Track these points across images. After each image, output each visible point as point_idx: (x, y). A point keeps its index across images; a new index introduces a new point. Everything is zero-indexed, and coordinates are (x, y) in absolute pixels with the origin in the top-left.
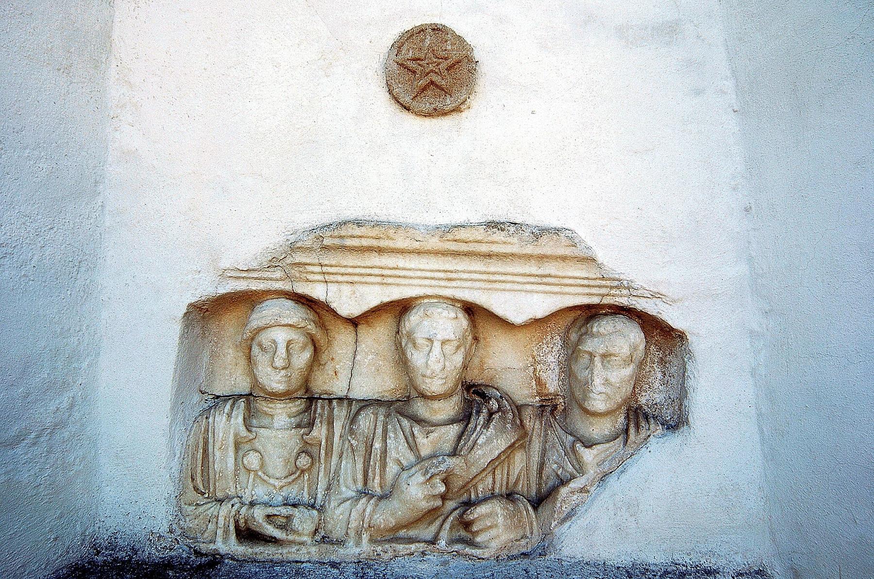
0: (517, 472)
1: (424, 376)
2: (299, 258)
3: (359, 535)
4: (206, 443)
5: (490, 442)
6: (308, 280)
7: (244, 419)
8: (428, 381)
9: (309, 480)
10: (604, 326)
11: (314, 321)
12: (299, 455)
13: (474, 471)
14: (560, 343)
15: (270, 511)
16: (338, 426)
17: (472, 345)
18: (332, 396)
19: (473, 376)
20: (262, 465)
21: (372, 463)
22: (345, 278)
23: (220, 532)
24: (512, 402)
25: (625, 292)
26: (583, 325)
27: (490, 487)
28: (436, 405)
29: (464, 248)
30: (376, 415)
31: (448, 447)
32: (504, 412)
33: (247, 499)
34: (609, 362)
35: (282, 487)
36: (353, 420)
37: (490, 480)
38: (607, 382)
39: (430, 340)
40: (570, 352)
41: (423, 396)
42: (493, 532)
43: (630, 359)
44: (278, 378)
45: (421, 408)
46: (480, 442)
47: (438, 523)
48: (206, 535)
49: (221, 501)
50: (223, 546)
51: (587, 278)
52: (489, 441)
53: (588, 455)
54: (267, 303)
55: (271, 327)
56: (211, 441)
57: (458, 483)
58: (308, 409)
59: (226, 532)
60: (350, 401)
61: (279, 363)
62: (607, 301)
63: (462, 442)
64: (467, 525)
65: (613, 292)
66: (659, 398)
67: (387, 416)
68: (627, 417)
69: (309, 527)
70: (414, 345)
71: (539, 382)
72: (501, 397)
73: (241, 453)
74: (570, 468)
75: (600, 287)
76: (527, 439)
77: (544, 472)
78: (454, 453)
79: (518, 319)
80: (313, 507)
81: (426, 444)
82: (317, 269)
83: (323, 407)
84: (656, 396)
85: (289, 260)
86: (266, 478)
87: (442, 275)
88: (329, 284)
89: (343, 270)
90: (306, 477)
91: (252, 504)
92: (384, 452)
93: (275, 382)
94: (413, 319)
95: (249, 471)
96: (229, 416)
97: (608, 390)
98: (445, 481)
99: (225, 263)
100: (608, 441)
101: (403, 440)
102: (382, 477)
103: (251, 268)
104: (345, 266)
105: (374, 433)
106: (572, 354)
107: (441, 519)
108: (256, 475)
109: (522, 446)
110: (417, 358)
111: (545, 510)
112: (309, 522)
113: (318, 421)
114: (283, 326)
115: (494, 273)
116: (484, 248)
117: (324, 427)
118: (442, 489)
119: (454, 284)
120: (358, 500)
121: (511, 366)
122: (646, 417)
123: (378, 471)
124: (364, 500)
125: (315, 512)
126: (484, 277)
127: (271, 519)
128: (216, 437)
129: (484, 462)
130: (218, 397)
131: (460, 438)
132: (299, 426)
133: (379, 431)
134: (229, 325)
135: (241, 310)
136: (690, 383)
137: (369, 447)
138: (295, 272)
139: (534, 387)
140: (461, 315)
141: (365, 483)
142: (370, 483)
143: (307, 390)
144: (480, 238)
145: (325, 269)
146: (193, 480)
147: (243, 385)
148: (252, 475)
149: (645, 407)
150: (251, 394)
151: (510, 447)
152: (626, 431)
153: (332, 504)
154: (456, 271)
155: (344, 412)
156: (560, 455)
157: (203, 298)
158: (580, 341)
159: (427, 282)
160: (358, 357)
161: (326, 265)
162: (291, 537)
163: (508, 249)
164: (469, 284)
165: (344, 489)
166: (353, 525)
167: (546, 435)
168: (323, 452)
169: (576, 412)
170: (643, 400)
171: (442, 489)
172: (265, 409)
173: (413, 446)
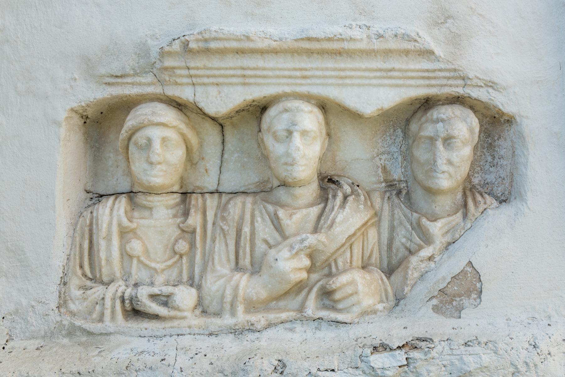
2: (169, 62)
3: (233, 306)
4: (91, 231)
6: (176, 84)
14: (402, 135)
18: (205, 191)
22: (211, 80)
37: (348, 254)
46: (338, 220)
49: (108, 284)
50: (111, 325)
51: (428, 71)
58: (184, 201)
67: (254, 203)
78: (316, 230)
82: (185, 72)
87: (298, 73)
89: (208, 72)
97: (451, 169)
98: (311, 256)
101: (269, 222)
107: (306, 290)
108: (140, 261)
111: (397, 277)
113: (192, 211)
129: (342, 239)
130: (101, 196)
133: (248, 217)
139: (381, 174)
140: (316, 110)
142: (241, 262)
147: (125, 186)
148: (135, 261)
152: (465, 205)
155: (215, 203)
156: (407, 230)
160: (226, 156)
161: (193, 68)
162: (173, 313)
165: (218, 267)
172: (145, 202)
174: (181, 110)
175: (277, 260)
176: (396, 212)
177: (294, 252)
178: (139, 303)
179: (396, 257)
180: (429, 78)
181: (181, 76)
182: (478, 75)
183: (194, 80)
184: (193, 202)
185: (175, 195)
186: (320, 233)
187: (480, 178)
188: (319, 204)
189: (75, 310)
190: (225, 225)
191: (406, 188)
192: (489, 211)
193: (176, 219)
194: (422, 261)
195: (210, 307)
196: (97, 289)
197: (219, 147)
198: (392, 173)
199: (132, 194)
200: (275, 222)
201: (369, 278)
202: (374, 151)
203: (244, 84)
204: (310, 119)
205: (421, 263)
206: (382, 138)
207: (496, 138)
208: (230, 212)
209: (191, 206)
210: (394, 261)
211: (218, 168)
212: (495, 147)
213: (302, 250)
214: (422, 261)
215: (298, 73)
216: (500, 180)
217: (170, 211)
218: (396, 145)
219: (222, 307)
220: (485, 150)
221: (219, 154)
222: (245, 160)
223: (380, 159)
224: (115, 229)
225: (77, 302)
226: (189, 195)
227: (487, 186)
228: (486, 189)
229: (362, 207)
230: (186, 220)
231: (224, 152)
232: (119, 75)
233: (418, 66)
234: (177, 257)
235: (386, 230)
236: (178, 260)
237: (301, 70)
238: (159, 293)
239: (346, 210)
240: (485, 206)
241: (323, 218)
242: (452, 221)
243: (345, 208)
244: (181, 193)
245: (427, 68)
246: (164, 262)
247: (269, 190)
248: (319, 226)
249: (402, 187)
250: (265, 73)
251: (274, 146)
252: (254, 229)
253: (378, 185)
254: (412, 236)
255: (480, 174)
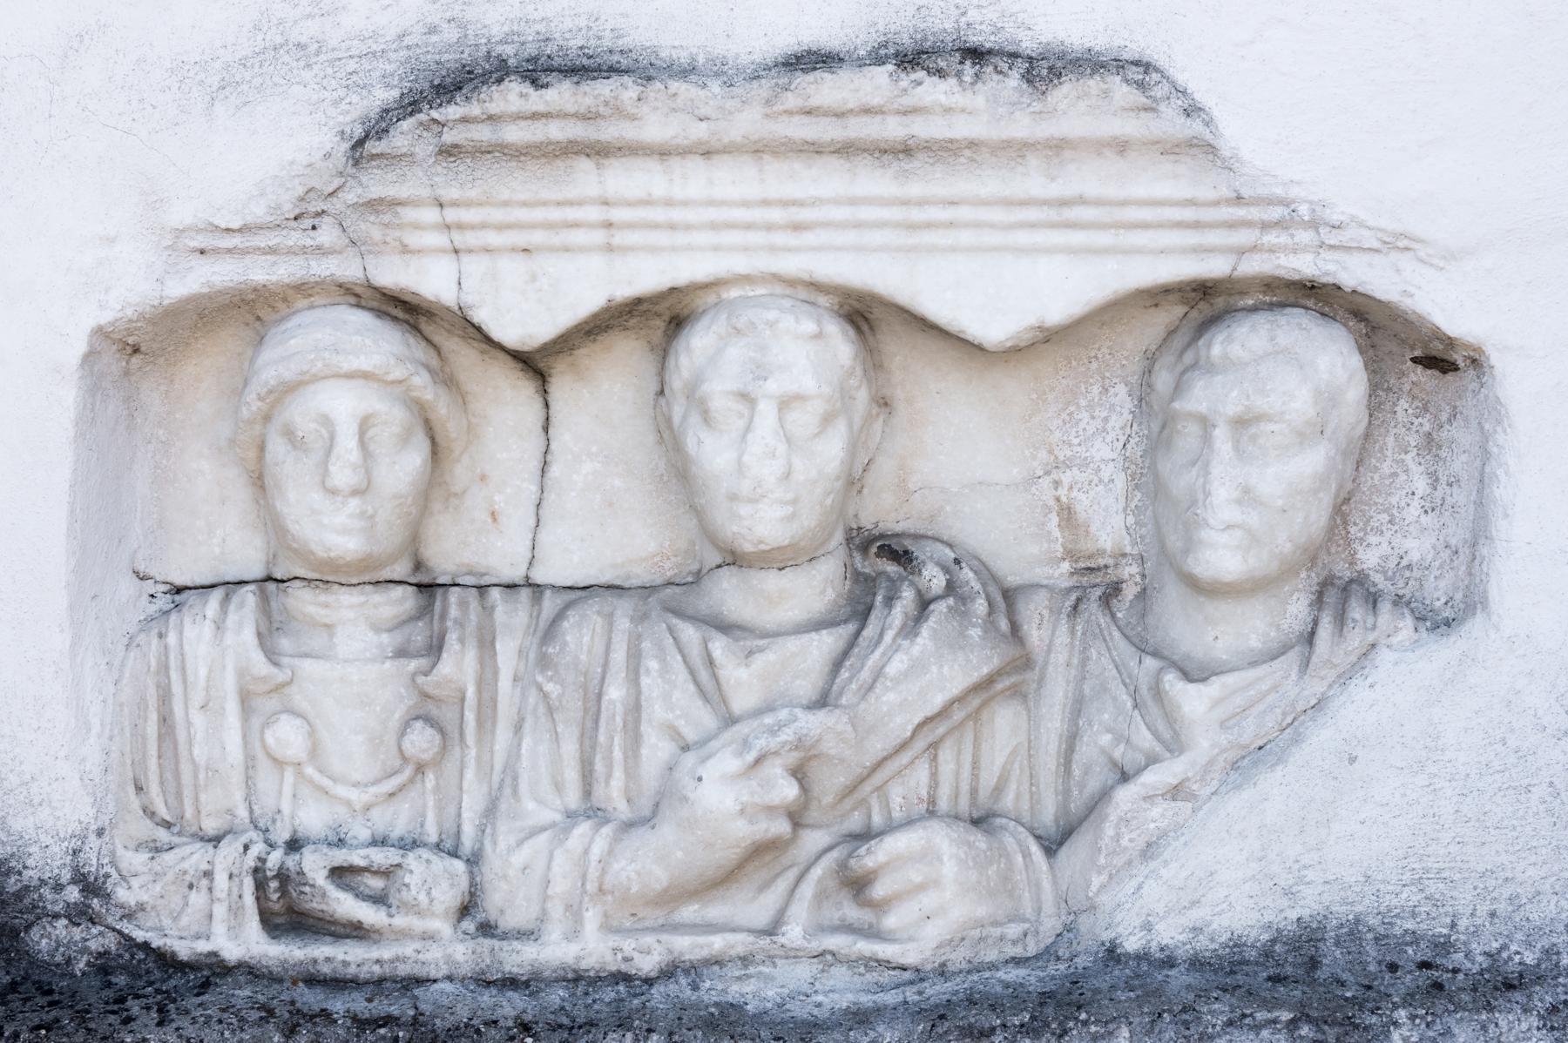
0: (1000, 760)
1: (733, 497)
3: (574, 913)
4: (165, 697)
5: (921, 669)
6: (405, 250)
7: (259, 635)
8: (744, 510)
9: (437, 789)
10: (1242, 339)
11: (427, 367)
12: (406, 726)
13: (877, 746)
14: (1129, 404)
15: (341, 857)
16: (507, 651)
17: (869, 419)
19: (882, 510)
20: (314, 751)
21: (602, 738)
23: (220, 911)
24: (987, 574)
25: (1305, 237)
26: (1189, 345)
27: (924, 793)
28: (771, 581)
29: (828, 131)
30: (610, 618)
31: (806, 688)
32: (964, 600)
33: (282, 835)
34: (1254, 438)
35: (367, 808)
36: (550, 633)
37: (922, 774)
38: (1247, 497)
39: (746, 398)
40: (1155, 427)
41: (734, 559)
42: (928, 900)
43: (1317, 430)
44: (341, 519)
45: (731, 595)
47: (782, 885)
48: (184, 921)
49: (216, 840)
51: (1191, 203)
52: (917, 667)
53: (1193, 700)
54: (296, 320)
55: (316, 379)
56: (177, 689)
57: (830, 782)
58: (425, 611)
59: (236, 911)
60: (537, 589)
61: (342, 476)
62: (1254, 266)
63: (844, 674)
64: (857, 885)
65: (1271, 238)
66: (1417, 548)
68: (1319, 601)
69: (448, 896)
70: (707, 418)
71: (1067, 514)
72: (957, 561)
73: (256, 722)
74: (1144, 739)
75: (1231, 225)
76: (1032, 676)
77: (1076, 757)
78: (822, 701)
79: (993, 330)
80: (454, 854)
81: (744, 679)
83: (463, 604)
84: (1410, 544)
85: (350, 197)
86: (326, 782)
87: (776, 215)
88: (465, 258)
89: (497, 215)
90: (430, 780)
91: (294, 845)
92: (635, 708)
93: (335, 530)
94: (698, 342)
95: (279, 763)
96: (219, 626)
97: (1253, 519)
98: (799, 773)
99: (182, 213)
100: (1253, 664)
101: (682, 675)
102: (631, 773)
103: (249, 219)
104: (506, 204)
105: (606, 665)
106: (1156, 424)
108: (300, 774)
109: (1017, 692)
110: (713, 453)
111: (1074, 854)
112: (445, 885)
113: (452, 638)
114: (350, 376)
115: (922, 203)
116: (892, 129)
117: (471, 657)
118: (788, 791)
119: (809, 238)
120: (567, 831)
121: (979, 472)
122: (1373, 600)
123: (618, 754)
124: (584, 828)
125: (459, 866)
126: (895, 214)
127: (348, 879)
128: (191, 678)
129: (903, 724)
130: (179, 590)
131: (837, 665)
132: (402, 653)
133: (619, 655)
134: (202, 373)
135: (227, 343)
136: (1501, 492)
137: (594, 701)
138: (369, 228)
139: (1057, 533)
141: (587, 793)
142: (599, 791)
143: (418, 566)
144: (876, 101)
145: (451, 215)
146: (139, 789)
147: (248, 559)
149: (1378, 578)
150: (269, 579)
151: (977, 688)
152: (1310, 637)
153: (502, 845)
154: (816, 202)
157: (129, 312)
158: (1178, 389)
159: (735, 237)
160: (555, 471)
161: (455, 204)
162: (400, 921)
163: (962, 129)
164: (850, 237)
165: (530, 805)
166: (560, 887)
167: (1084, 662)
168: (470, 716)
169: (1171, 598)
170: (1370, 558)
171: (788, 791)
173: (711, 690)
174: (415, 328)
175: (700, 779)
176: (1093, 653)
177: (751, 757)
178: (307, 889)
179: (1081, 792)
180: (1197, 225)
181: (417, 226)
182: (1362, 215)
183: (459, 239)
184: (454, 612)
185: (399, 591)
186: (836, 706)
187: (1385, 549)
188: (846, 621)
189: (133, 903)
190: (550, 679)
191: (1138, 579)
192: (1384, 657)
193: (403, 661)
194: (1146, 798)
195: (509, 911)
196: (188, 849)
197: (535, 442)
198: (1093, 529)
199: (271, 586)
200: (704, 676)
201: (983, 846)
202: (1034, 458)
203: (610, 248)
204: (810, 354)
205: (1145, 806)
206: (1064, 416)
207: (1444, 417)
208: (565, 643)
209: (449, 624)
210: (1076, 804)
211: (533, 509)
212: (1440, 447)
213: (776, 753)
214: (1146, 798)
215: (776, 215)
216: (1446, 554)
217: (385, 638)
218: (1109, 439)
219: (544, 911)
220: (1408, 458)
221: (535, 465)
222: (617, 482)
223: (1057, 484)
224: (230, 684)
225: (135, 883)
226: (440, 591)
227: (1407, 574)
228: (1401, 584)
229: (975, 633)
230: (434, 665)
231: (549, 458)
232: (235, 226)
233: (1164, 190)
234: (408, 772)
235: (1057, 709)
236: (412, 780)
237: (785, 203)
238: (362, 863)
239: (919, 640)
240: (1371, 638)
241: (847, 663)
242: (1259, 679)
243: (916, 635)
244: (419, 586)
245: (1189, 196)
246: (373, 784)
247: (690, 579)
248: (835, 687)
249: (1126, 576)
250: (677, 215)
251: (700, 442)
252: (639, 693)
253: (1048, 571)
254: (1133, 726)
255: (1388, 534)
